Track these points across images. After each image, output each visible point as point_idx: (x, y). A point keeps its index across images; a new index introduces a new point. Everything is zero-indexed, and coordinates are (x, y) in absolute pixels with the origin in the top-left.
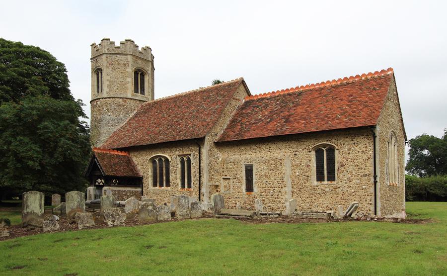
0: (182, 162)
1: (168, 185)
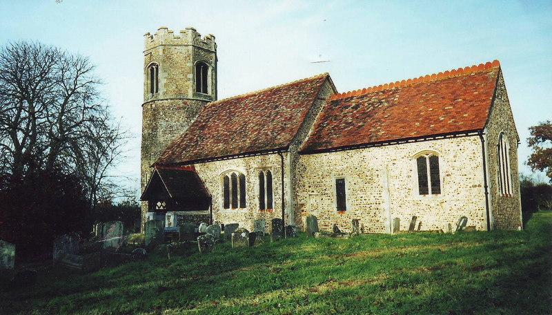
0: (261, 177)
1: (243, 206)
